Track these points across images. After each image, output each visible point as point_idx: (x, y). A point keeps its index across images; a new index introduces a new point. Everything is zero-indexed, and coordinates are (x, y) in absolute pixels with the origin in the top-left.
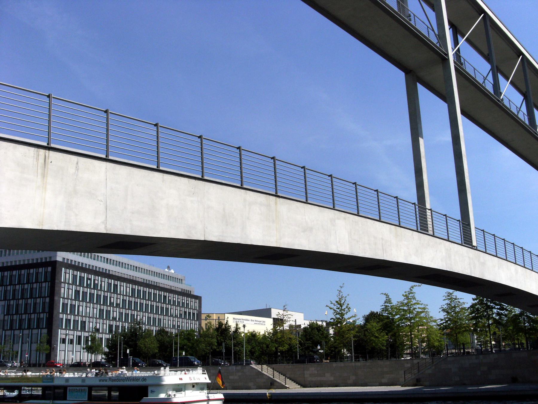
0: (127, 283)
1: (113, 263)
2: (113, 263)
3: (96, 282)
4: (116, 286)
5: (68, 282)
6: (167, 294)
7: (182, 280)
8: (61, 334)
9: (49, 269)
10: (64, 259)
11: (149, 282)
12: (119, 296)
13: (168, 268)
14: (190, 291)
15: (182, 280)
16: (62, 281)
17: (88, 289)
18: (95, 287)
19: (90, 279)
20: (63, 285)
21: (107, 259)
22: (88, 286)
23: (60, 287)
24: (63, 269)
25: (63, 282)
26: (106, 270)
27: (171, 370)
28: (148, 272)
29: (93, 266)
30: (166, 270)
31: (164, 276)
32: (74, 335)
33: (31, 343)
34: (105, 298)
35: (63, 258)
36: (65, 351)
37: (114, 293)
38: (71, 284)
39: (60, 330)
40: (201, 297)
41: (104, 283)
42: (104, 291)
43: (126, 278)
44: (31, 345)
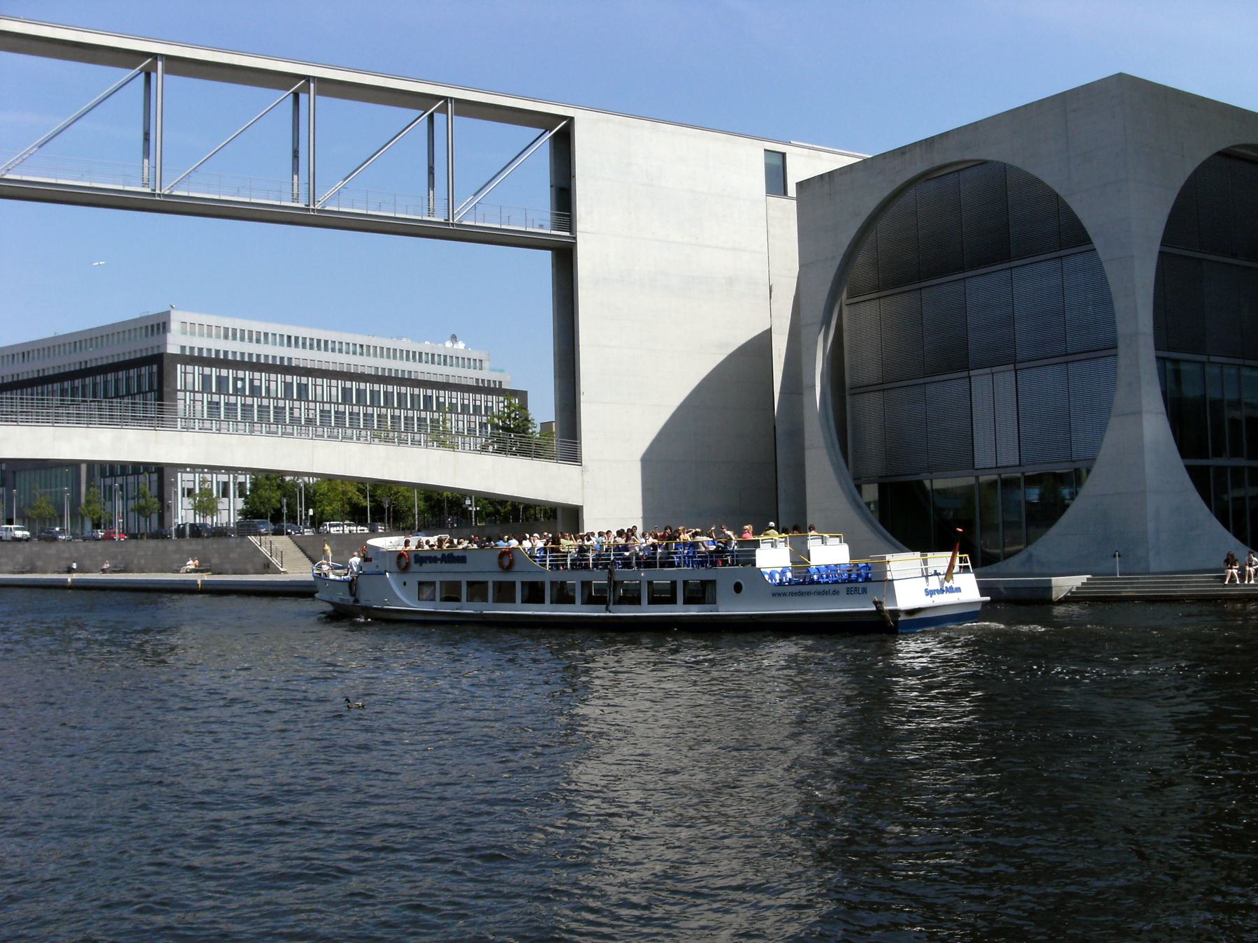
0: (413, 387)
1: (304, 344)
2: (304, 344)
3: (442, 400)
4: (303, 389)
5: (275, 396)
6: (433, 393)
7: (481, 361)
8: (182, 481)
9: (155, 368)
10: (183, 348)
11: (484, 384)
12: (312, 405)
13: (454, 338)
14: (500, 382)
15: (481, 361)
16: (179, 388)
17: (239, 398)
18: (255, 391)
19: (243, 380)
20: (180, 395)
21: (289, 337)
22: (237, 392)
23: (175, 400)
24: (179, 366)
25: (180, 391)
26: (489, 381)
27: (748, 556)
28: (392, 353)
29: (397, 371)
30: (448, 344)
31: (418, 357)
32: (194, 481)
33: (127, 499)
34: (279, 411)
35: (182, 346)
36: (229, 510)
37: (299, 399)
38: (198, 392)
39: (179, 474)
40: (525, 393)
41: (277, 382)
42: (277, 398)
43: (318, 369)
44: (1153, 574)
